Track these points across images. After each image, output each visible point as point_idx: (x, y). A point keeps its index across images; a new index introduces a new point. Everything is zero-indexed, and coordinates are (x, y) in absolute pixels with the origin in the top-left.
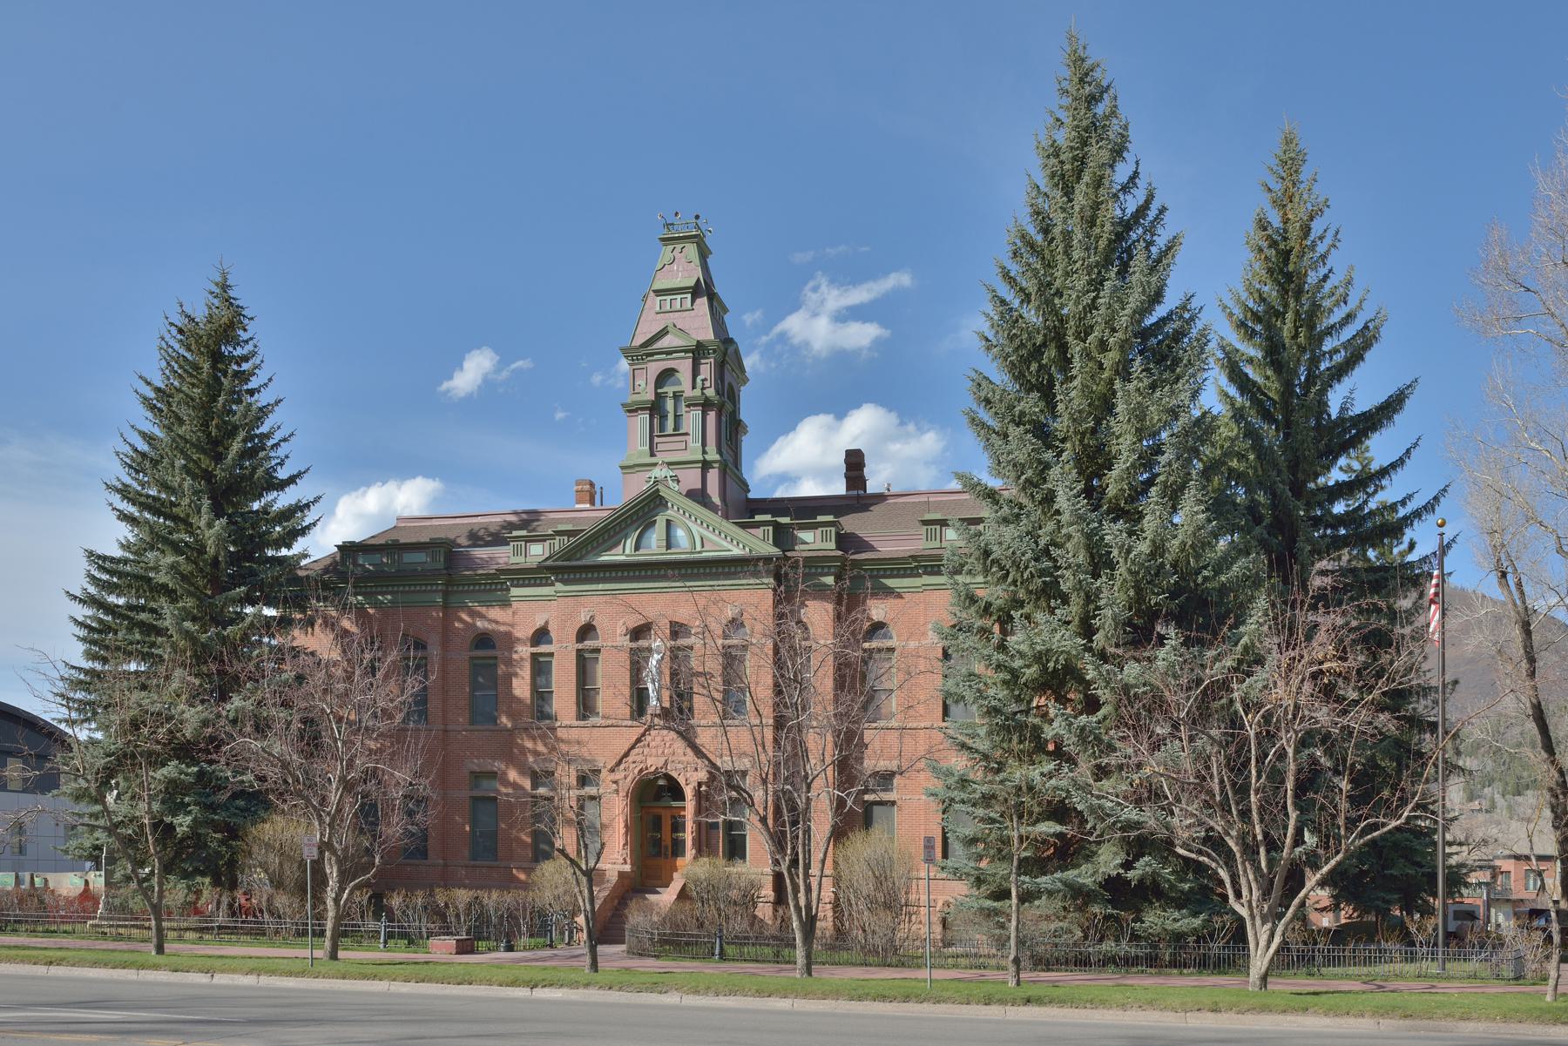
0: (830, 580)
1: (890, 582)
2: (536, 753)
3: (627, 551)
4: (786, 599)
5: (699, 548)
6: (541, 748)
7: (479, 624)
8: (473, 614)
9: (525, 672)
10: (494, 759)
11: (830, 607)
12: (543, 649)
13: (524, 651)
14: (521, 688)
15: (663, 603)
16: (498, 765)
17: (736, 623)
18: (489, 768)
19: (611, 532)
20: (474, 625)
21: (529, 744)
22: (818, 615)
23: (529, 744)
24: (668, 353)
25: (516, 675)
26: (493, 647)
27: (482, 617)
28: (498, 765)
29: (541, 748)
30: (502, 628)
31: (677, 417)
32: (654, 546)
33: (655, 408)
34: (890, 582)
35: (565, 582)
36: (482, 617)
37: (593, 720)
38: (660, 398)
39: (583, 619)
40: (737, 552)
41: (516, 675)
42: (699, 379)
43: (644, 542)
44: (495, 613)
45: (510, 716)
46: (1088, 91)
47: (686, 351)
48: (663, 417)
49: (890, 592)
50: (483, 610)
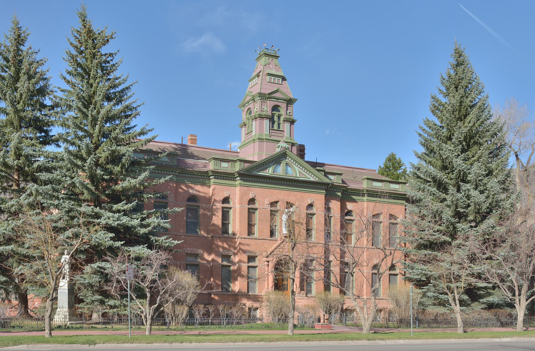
0: (339, 194)
1: (354, 197)
2: (224, 248)
3: (270, 172)
4: (328, 199)
5: (298, 176)
6: (226, 245)
7: (191, 191)
8: (187, 186)
9: (219, 214)
10: (197, 248)
11: (340, 203)
12: (226, 205)
13: (219, 205)
14: (217, 220)
15: (282, 194)
16: (200, 251)
17: (311, 206)
18: (196, 252)
19: (265, 164)
20: (188, 192)
21: (220, 244)
22: (335, 205)
23: (220, 244)
24: (277, 99)
25: (215, 215)
26: (196, 202)
27: (192, 188)
28: (200, 251)
29: (226, 245)
30: (202, 194)
31: (279, 124)
32: (280, 171)
33: (271, 119)
34: (354, 197)
35: (244, 180)
36: (192, 188)
37: (251, 237)
38: (273, 115)
39: (251, 196)
40: (312, 179)
41: (215, 215)
42: (288, 112)
43: (276, 170)
44: (198, 187)
45: (129, 235)
46: (459, 54)
47: (284, 100)
48: (273, 123)
49: (354, 201)
50: (193, 186)
